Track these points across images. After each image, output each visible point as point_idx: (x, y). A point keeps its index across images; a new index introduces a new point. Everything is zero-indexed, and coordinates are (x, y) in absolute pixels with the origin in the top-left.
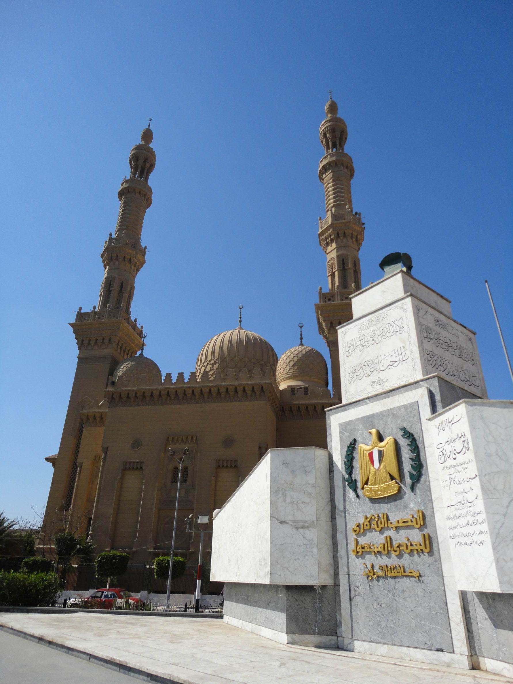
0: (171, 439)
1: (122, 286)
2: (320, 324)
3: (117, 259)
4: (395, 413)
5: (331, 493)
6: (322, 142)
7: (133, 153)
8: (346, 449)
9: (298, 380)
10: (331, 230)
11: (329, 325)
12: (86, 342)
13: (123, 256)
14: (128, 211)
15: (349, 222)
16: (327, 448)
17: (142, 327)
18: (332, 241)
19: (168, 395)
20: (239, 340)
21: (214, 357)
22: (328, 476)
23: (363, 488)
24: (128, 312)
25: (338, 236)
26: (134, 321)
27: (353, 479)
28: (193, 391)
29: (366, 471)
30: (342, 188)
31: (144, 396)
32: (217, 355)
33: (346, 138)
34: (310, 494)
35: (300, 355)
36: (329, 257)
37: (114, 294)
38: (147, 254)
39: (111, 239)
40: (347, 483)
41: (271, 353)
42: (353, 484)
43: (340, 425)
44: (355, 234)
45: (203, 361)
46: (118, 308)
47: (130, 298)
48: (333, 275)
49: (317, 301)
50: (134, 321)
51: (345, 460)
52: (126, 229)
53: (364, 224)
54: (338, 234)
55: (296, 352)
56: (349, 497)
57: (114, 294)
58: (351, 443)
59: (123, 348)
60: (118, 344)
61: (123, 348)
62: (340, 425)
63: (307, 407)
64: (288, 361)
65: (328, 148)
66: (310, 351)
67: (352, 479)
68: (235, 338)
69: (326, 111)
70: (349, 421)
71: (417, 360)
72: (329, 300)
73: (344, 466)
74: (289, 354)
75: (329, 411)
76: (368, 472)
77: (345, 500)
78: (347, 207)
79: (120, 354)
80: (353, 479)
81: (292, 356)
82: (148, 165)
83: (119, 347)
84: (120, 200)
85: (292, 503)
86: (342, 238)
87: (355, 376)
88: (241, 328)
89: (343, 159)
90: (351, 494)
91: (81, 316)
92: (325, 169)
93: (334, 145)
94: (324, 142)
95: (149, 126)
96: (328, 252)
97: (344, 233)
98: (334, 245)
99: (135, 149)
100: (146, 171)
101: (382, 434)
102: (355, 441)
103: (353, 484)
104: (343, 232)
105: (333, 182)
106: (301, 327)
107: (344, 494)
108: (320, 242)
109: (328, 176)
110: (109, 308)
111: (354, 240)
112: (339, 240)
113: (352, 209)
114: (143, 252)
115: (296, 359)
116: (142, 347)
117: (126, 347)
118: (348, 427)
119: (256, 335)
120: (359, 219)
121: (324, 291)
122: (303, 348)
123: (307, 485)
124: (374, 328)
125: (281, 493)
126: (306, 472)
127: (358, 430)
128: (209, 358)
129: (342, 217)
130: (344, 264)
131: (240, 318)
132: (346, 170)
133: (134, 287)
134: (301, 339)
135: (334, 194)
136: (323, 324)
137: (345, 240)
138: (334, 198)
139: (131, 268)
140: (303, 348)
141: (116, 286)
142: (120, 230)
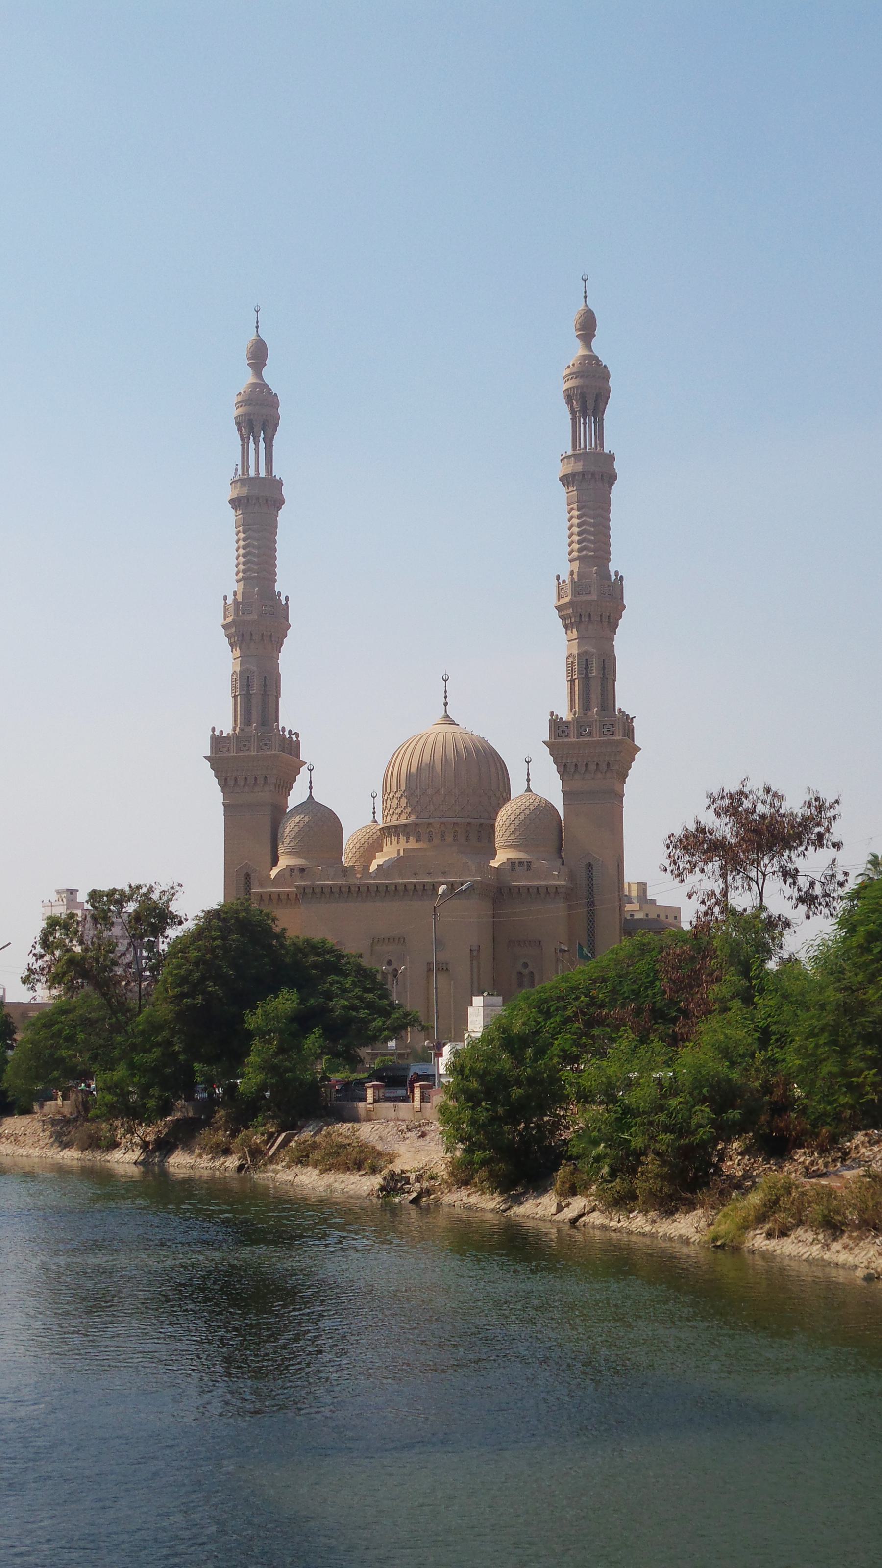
7: (241, 411)
9: (520, 851)
11: (562, 770)
12: (231, 782)
13: (258, 625)
63: (528, 888)
91: (218, 742)
106: (528, 763)
111: (605, 624)
115: (517, 822)
131: (446, 697)
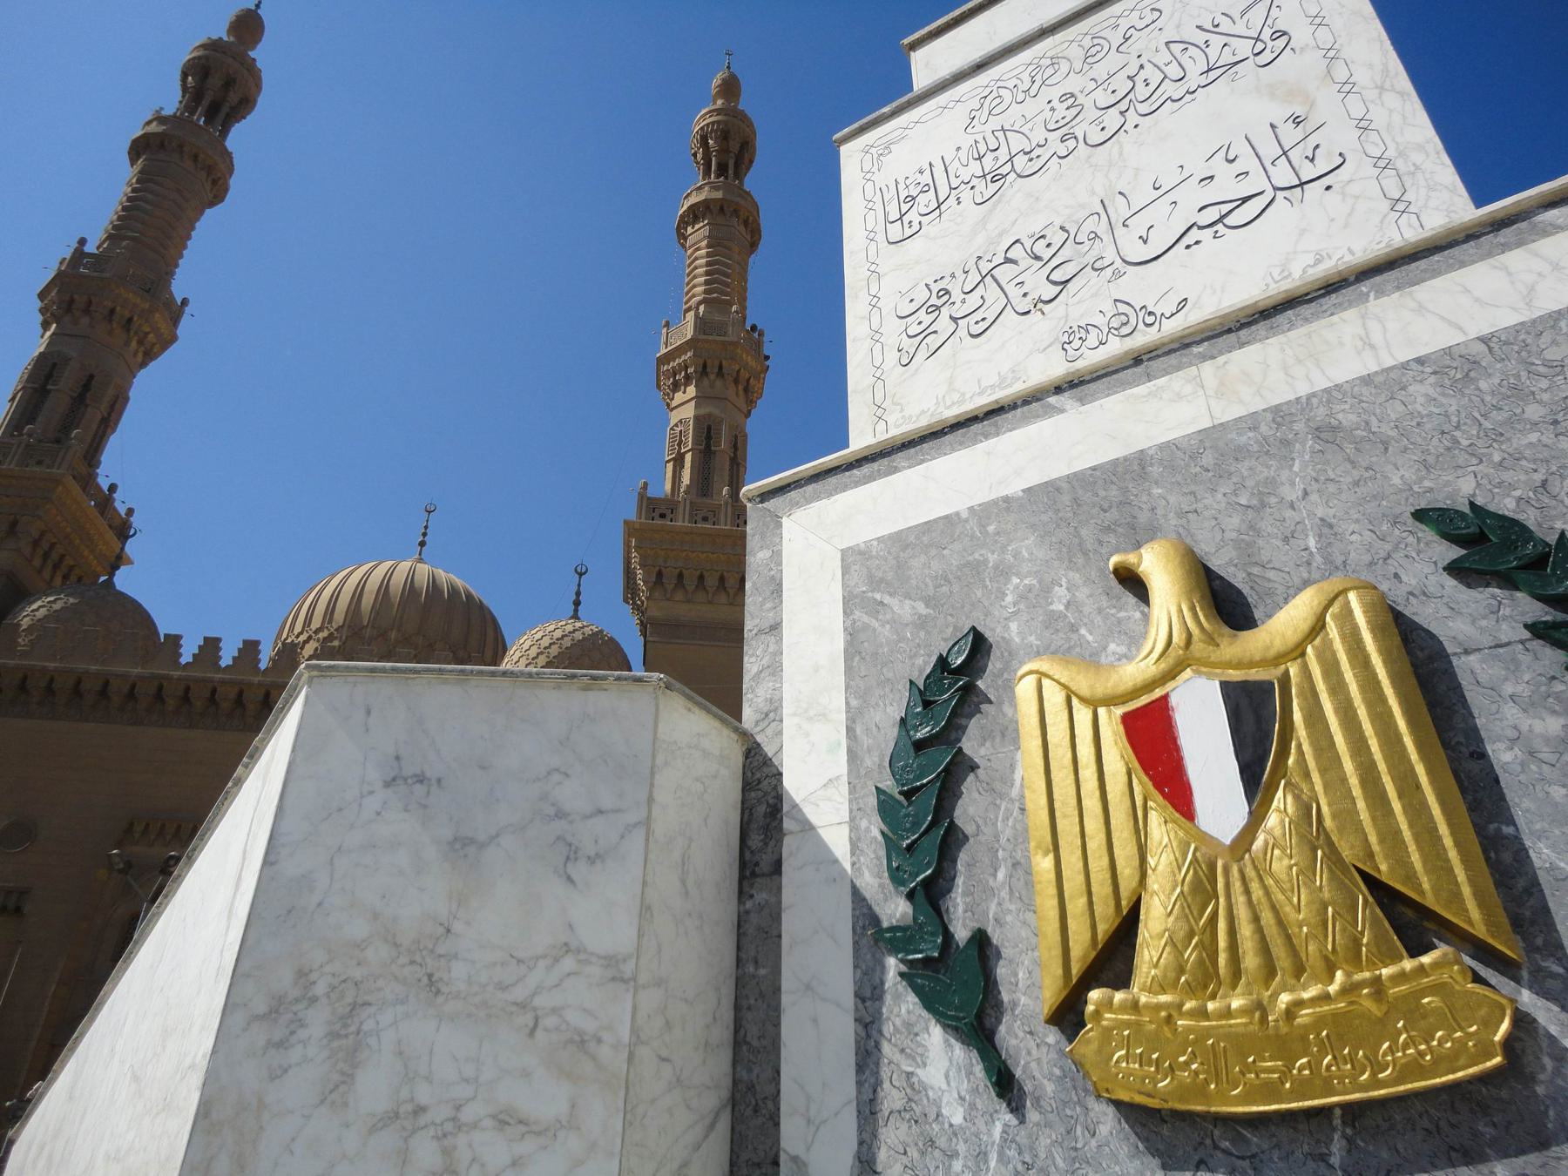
0: (139, 828)
1: (87, 387)
2: (629, 575)
3: (87, 311)
4: (1347, 418)
5: (739, 1041)
6: (695, 155)
7: (201, 53)
8: (892, 708)
10: (689, 354)
14: (150, 196)
15: (735, 344)
16: (737, 713)
17: (130, 512)
18: (688, 379)
19: (159, 696)
20: (411, 588)
21: (330, 621)
22: (729, 910)
23: (1069, 1016)
24: (92, 456)
25: (703, 371)
26: (105, 488)
27: (961, 934)
28: (241, 693)
29: (1099, 864)
30: (727, 266)
31: (77, 691)
32: (339, 617)
33: (751, 162)
34: (581, 1042)
35: (567, 642)
36: (675, 417)
37: (58, 401)
38: (185, 321)
39: (79, 254)
40: (892, 964)
41: (490, 632)
42: (961, 982)
43: (852, 558)
44: (744, 375)
45: (298, 629)
46: (58, 441)
47: (108, 423)
48: (679, 461)
49: (632, 515)
50: (105, 488)
51: (889, 784)
52: (133, 239)
53: (767, 358)
54: (705, 366)
55: (558, 634)
56: (914, 1088)
57: (58, 401)
58: (942, 662)
59: (55, 556)
60: (36, 543)
61: (55, 556)
62: (852, 558)
64: (533, 652)
65: (707, 173)
66: (594, 634)
67: (948, 936)
68: (399, 579)
69: (714, 92)
70: (927, 527)
71: (1418, 158)
72: (663, 516)
73: (874, 827)
74: (538, 636)
75: (766, 496)
76: (1128, 872)
77: (868, 1112)
78: (734, 308)
79: (40, 572)
80: (961, 934)
81: (546, 642)
82: (233, 98)
83: (40, 552)
84: (133, 162)
85: (405, 1117)
86: (712, 377)
87: (943, 324)
88: (421, 560)
89: (742, 202)
90: (936, 1062)
92: (694, 214)
93: (722, 170)
94: (699, 156)
95: (258, 6)
96: (674, 404)
97: (721, 367)
98: (691, 391)
99: (203, 46)
100: (225, 110)
101: (1237, 579)
102: (979, 645)
103: (961, 982)
104: (717, 363)
105: (708, 246)
106: (581, 575)
107: (867, 1057)
108: (658, 380)
109: (699, 233)
110: (30, 436)
112: (706, 382)
113: (744, 318)
114: (175, 311)
116: (118, 560)
117: (62, 557)
118: (917, 563)
119: (459, 582)
120: (759, 344)
121: (651, 493)
122: (578, 625)
123: (568, 963)
124: (1073, 84)
125: (318, 1021)
126: (570, 858)
127: (1003, 572)
128: (316, 624)
129: (720, 329)
130: (709, 438)
132: (742, 228)
133: (127, 400)
134: (577, 603)
135: (707, 273)
136: (639, 573)
137: (719, 383)
138: (706, 283)
139: (127, 343)
140: (578, 625)
141: (66, 383)
142: (114, 237)
